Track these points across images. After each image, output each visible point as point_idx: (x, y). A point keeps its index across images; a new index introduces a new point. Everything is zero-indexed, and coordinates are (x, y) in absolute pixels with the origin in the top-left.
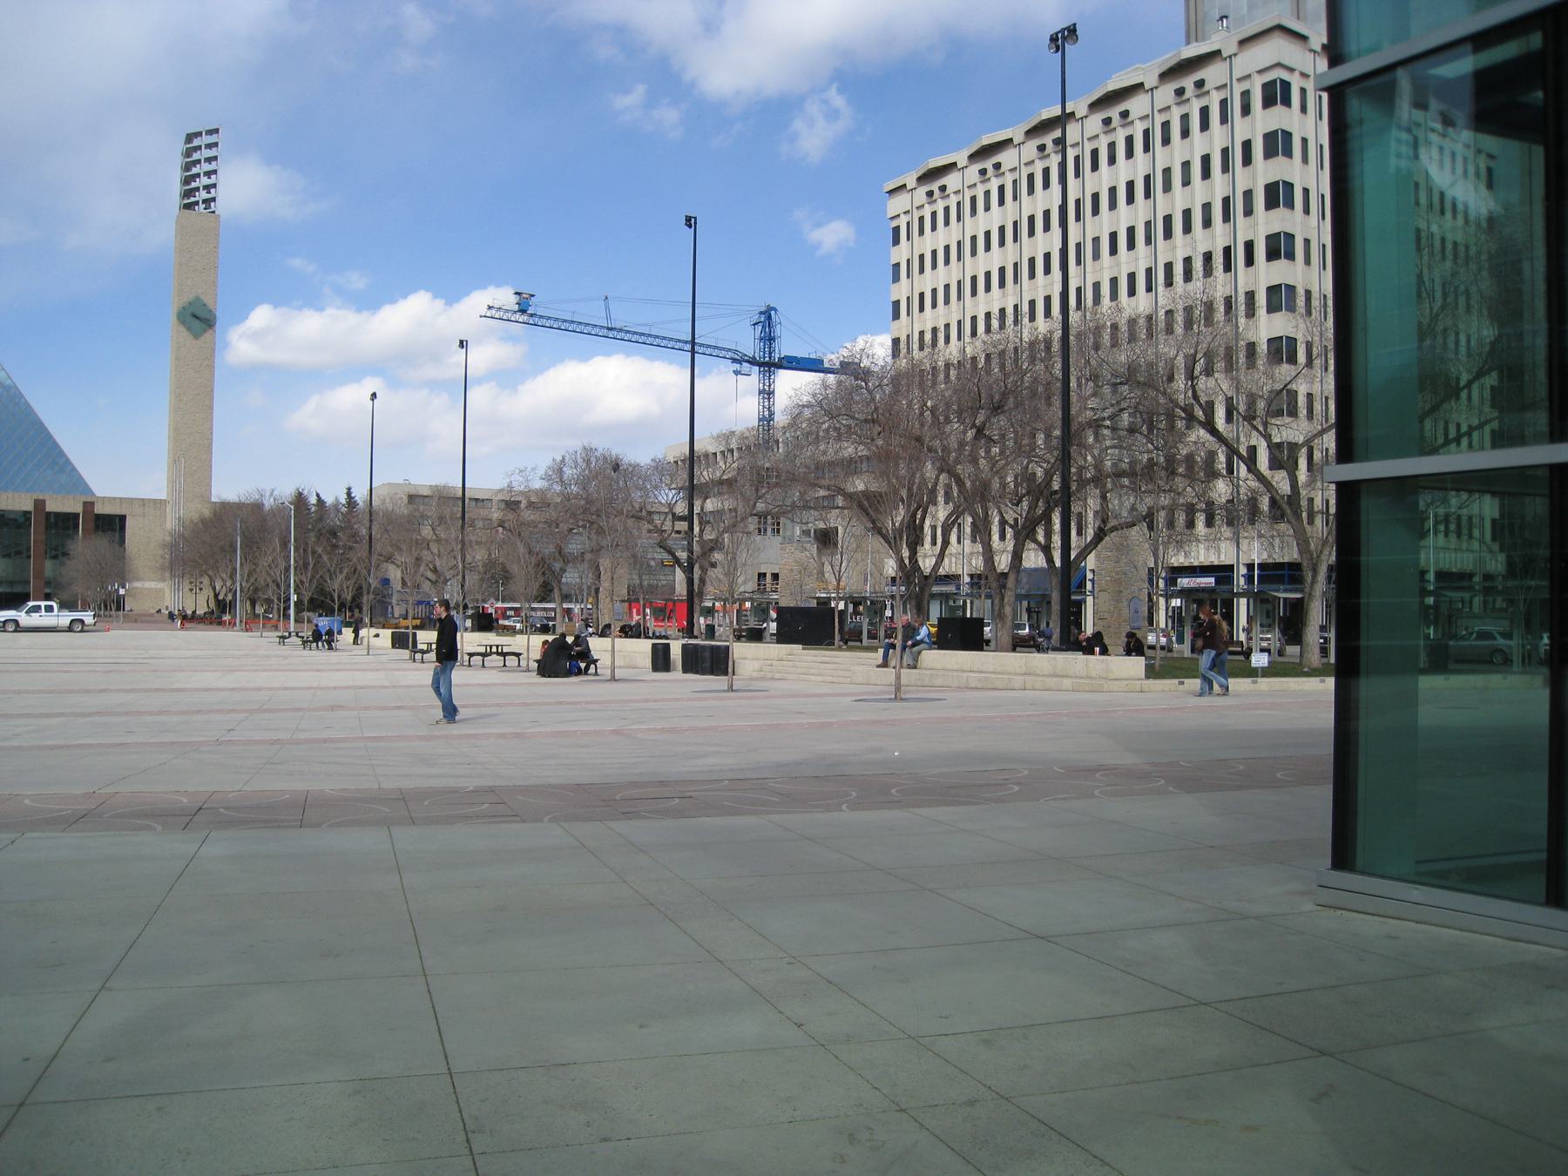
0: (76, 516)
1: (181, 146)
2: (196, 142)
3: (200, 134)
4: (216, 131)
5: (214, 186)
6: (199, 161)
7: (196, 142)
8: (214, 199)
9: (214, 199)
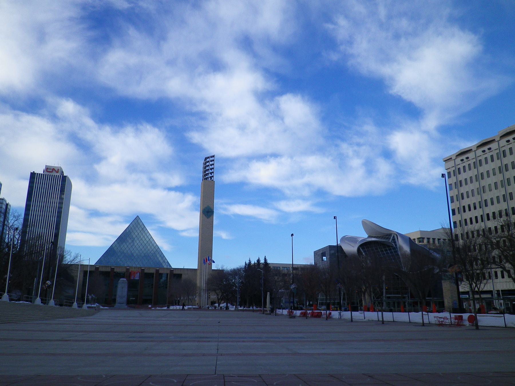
0: (153, 274)
1: (203, 161)
2: (208, 160)
3: (209, 158)
4: (214, 156)
5: (213, 172)
6: (208, 170)
7: (208, 160)
8: (213, 177)
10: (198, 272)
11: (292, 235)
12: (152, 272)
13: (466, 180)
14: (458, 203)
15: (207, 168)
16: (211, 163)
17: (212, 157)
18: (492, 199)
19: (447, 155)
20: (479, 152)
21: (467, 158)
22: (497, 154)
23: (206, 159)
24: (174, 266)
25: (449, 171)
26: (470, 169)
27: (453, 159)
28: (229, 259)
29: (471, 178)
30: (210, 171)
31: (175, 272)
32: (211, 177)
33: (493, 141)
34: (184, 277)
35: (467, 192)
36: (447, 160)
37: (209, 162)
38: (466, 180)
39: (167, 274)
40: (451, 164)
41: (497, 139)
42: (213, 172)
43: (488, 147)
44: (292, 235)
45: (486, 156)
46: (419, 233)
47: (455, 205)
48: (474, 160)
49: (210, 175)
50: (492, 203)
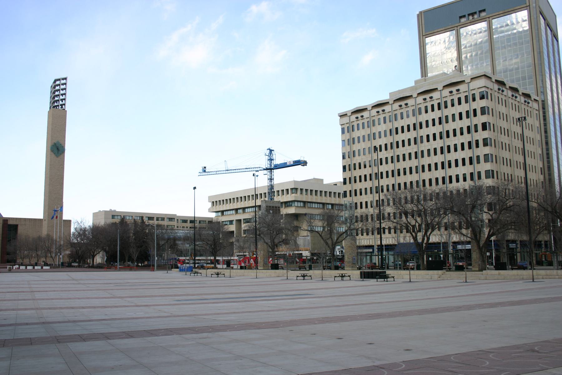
2: (58, 83)
3: (59, 80)
4: (66, 79)
7: (58, 83)
8: (64, 104)
9: (64, 104)
10: (45, 224)
11: (195, 188)
12: (232, 230)
13: (359, 138)
14: (349, 160)
15: (56, 99)
16: (62, 92)
17: (63, 79)
18: (455, 145)
19: (343, 110)
20: (420, 99)
21: (362, 116)
22: (348, 127)
24: (4, 216)
25: (343, 126)
26: (363, 128)
27: (390, 103)
28: (81, 211)
29: (364, 136)
30: (61, 97)
31: (10, 223)
32: (62, 105)
33: (410, 97)
34: (20, 230)
35: (359, 150)
36: (342, 116)
37: (59, 85)
38: (380, 133)
40: (346, 120)
41: (369, 108)
42: (65, 99)
43: (405, 102)
44: (195, 188)
45: (358, 122)
46: (104, 213)
47: (348, 161)
48: (369, 120)
49: (61, 103)
50: (456, 150)
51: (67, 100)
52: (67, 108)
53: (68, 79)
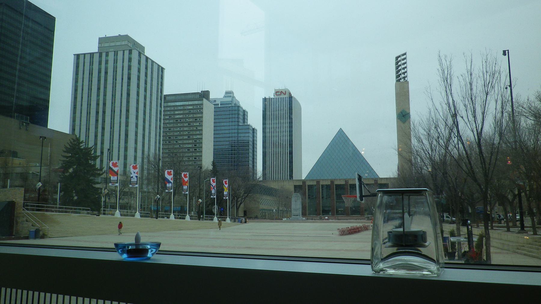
2: (399, 59)
3: (400, 56)
4: (405, 54)
5: (406, 72)
17: (403, 55)
23: (397, 58)
37: (400, 61)
39: (92, 55)
49: (403, 76)
51: (408, 67)
52: (409, 79)
53: (407, 54)
